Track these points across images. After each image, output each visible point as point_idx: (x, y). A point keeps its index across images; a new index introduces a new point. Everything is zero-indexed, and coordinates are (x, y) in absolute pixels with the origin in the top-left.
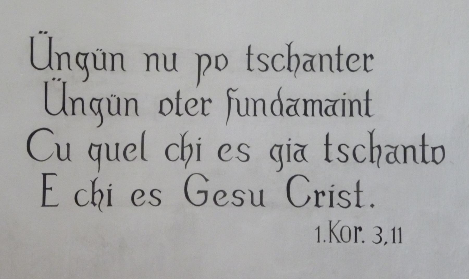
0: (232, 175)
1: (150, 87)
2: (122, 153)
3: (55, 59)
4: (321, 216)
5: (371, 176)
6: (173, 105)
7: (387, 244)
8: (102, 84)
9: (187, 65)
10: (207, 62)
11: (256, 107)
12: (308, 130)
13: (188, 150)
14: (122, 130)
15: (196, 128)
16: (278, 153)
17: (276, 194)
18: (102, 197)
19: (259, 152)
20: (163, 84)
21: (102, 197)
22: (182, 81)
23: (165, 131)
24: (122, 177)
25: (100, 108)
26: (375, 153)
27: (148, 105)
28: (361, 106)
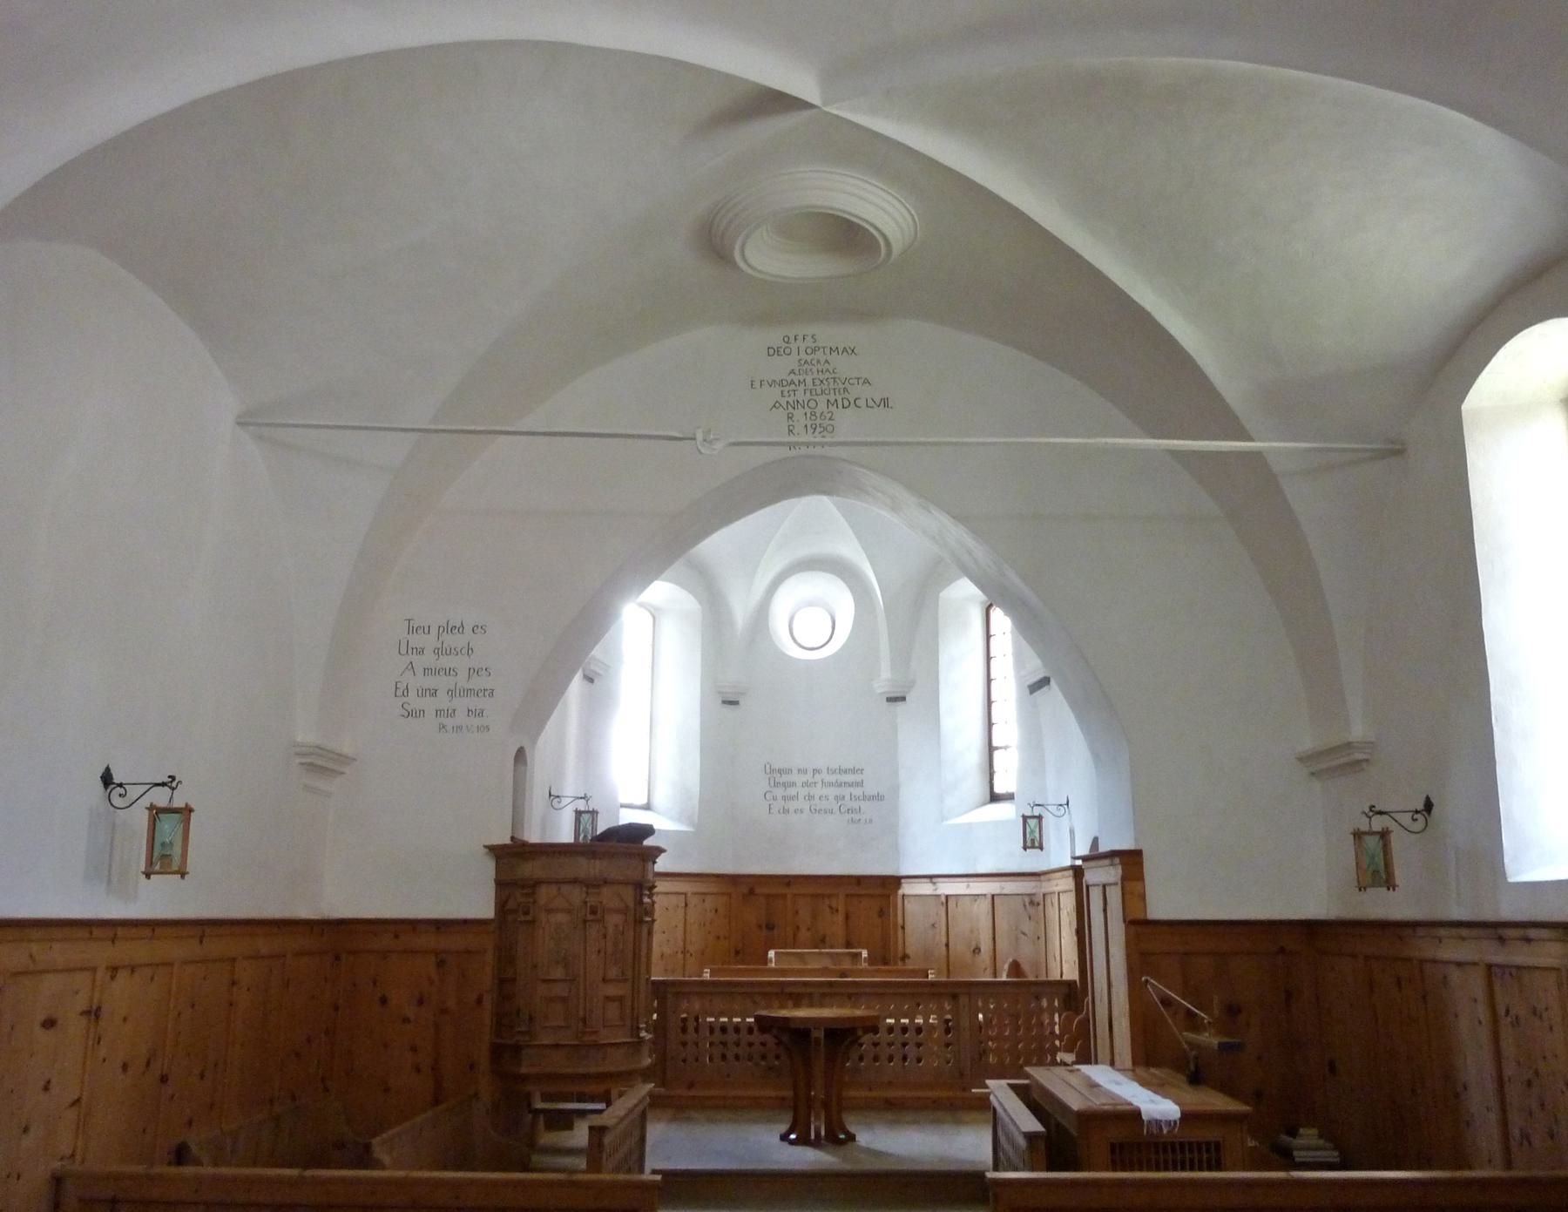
0: (824, 805)
1: (799, 779)
2: (792, 798)
3: (772, 771)
4: (848, 816)
5: (864, 805)
6: (806, 784)
7: (42, 1083)
8: (785, 778)
9: (810, 773)
10: (816, 771)
11: (831, 784)
12: (846, 791)
13: (810, 797)
14: (792, 791)
15: (813, 791)
16: (837, 798)
17: (836, 809)
18: (786, 811)
19: (831, 798)
20: (803, 778)
21: (786, 811)
22: (809, 777)
23: (803, 792)
24: (792, 805)
25: (786, 785)
26: (865, 798)
27: (799, 784)
28: (860, 784)
